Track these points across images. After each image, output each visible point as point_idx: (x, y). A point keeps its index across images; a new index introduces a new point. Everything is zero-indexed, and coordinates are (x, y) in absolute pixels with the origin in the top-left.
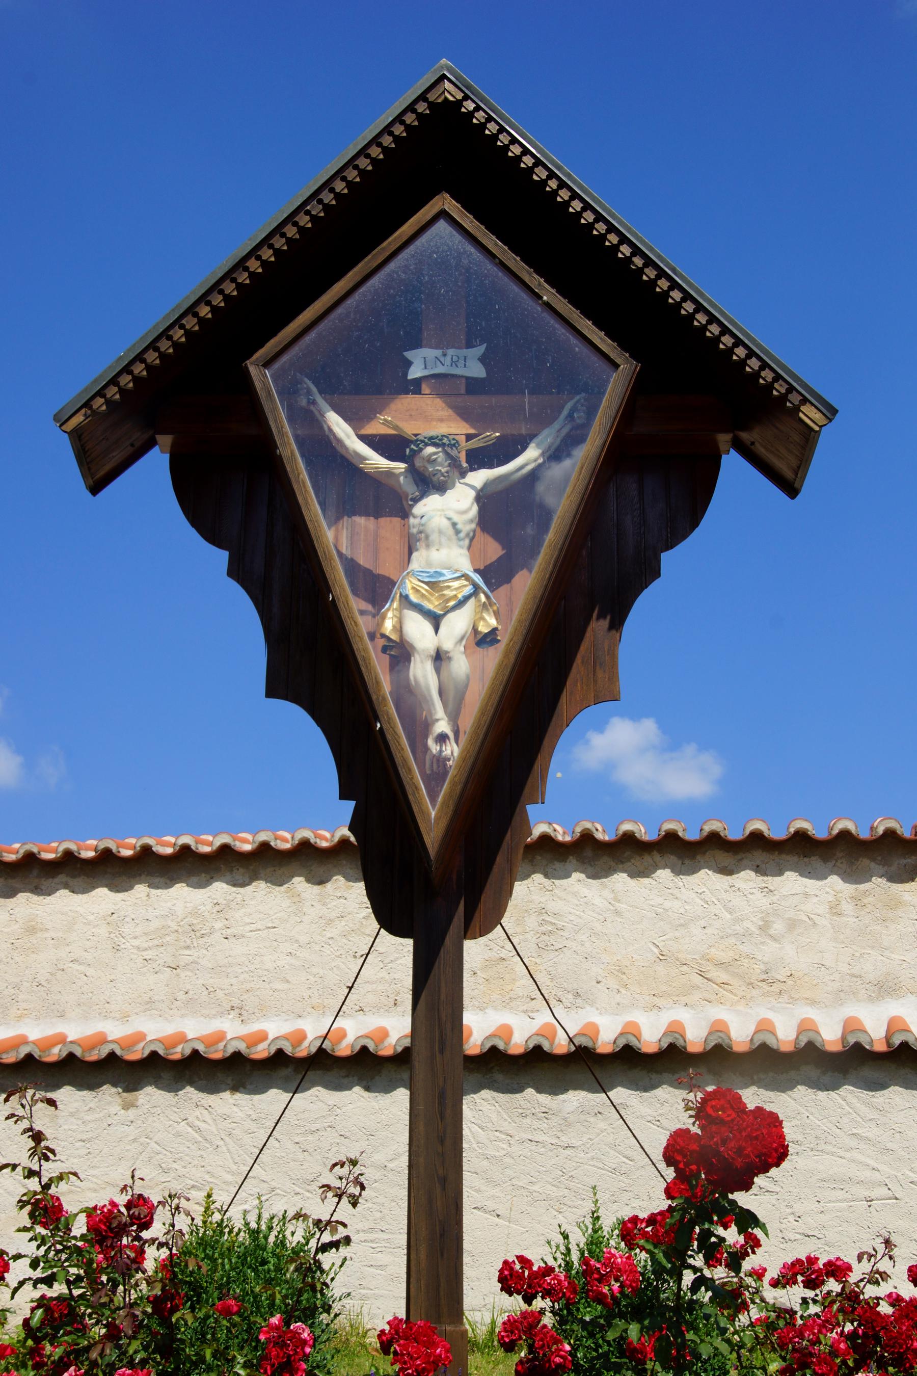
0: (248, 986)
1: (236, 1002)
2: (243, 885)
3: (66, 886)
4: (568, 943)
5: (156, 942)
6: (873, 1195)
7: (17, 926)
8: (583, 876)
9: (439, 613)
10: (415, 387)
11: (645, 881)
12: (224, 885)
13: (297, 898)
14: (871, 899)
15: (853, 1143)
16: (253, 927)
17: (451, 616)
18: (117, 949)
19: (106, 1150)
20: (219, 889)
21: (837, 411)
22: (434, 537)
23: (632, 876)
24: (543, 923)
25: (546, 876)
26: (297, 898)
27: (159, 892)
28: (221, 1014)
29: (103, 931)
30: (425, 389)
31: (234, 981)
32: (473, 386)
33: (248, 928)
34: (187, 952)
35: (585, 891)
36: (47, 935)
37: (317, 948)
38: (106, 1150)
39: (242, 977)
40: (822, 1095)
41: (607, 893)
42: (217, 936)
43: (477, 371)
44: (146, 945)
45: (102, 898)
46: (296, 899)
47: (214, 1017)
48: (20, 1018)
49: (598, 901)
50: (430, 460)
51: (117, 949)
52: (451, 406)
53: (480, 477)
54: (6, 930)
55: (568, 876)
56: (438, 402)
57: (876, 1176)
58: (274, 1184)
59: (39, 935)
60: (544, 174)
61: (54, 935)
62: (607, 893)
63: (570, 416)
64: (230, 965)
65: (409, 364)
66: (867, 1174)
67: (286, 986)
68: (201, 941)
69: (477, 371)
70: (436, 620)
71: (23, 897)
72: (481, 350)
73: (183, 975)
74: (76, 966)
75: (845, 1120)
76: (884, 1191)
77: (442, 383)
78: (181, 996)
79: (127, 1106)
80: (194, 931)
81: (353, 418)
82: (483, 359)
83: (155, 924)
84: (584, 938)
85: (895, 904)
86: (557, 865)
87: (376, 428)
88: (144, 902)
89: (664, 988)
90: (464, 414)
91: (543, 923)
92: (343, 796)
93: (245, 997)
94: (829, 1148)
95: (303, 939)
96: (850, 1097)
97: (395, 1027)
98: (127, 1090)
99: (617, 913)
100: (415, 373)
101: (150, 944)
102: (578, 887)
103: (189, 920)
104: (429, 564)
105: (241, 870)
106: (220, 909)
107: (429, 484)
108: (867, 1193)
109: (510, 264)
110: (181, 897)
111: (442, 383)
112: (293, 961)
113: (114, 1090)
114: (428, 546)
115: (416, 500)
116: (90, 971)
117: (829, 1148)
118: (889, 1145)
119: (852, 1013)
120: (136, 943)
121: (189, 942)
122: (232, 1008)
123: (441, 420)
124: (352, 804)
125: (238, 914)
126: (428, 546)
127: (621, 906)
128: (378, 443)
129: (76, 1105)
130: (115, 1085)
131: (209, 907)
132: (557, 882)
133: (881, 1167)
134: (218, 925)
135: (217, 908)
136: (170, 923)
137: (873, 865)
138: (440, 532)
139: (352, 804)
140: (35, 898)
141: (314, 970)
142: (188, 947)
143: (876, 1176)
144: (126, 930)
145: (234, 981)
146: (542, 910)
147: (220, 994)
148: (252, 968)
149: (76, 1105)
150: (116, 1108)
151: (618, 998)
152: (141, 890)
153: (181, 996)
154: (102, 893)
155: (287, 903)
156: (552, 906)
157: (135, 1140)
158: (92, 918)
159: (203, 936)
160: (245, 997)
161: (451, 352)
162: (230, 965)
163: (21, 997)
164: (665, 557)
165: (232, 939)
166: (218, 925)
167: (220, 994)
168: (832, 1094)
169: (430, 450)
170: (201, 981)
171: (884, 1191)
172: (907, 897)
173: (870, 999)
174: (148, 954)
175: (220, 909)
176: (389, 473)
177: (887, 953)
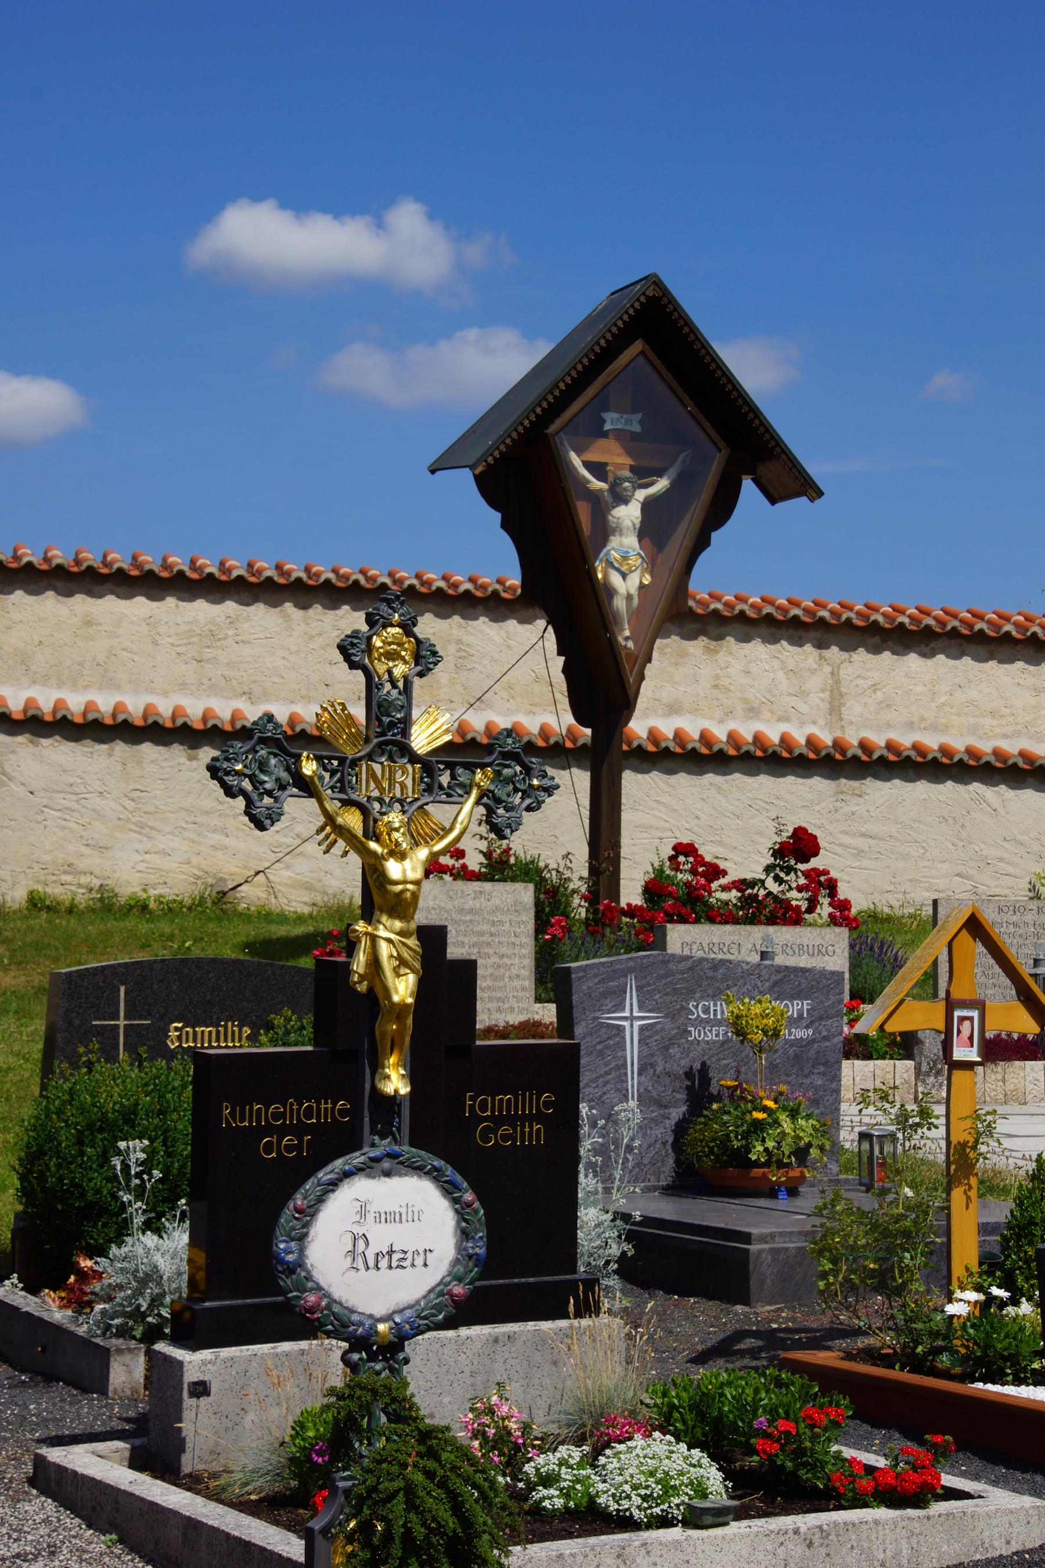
0: (255, 678)
1: (246, 689)
2: (248, 605)
3: (113, 593)
4: (477, 666)
5: (185, 641)
6: (664, 836)
7: (76, 619)
8: (487, 620)
9: (625, 570)
10: (605, 435)
11: (529, 626)
12: (234, 604)
13: (287, 617)
14: (669, 650)
15: (655, 805)
16: (256, 636)
17: (632, 575)
18: (155, 643)
19: (178, 787)
20: (230, 607)
21: (822, 494)
22: (625, 531)
23: (521, 622)
24: (460, 650)
25: (463, 617)
26: (287, 617)
27: (185, 604)
28: (237, 697)
29: (144, 629)
30: (611, 436)
31: (244, 674)
32: (634, 436)
33: (252, 637)
34: (208, 650)
35: (488, 630)
36: (100, 628)
37: (303, 655)
38: (178, 787)
39: (250, 672)
40: (640, 776)
41: (502, 633)
42: (230, 641)
43: (636, 428)
44: (177, 643)
45: (140, 606)
46: (287, 619)
47: (231, 698)
48: (86, 687)
49: (496, 638)
50: (625, 489)
51: (155, 643)
52: (623, 447)
53: (641, 494)
54: (69, 621)
55: (477, 619)
56: (617, 444)
57: (667, 825)
58: (295, 815)
59: (95, 627)
60: (682, 323)
61: (107, 629)
62: (502, 633)
63: (684, 461)
64: (241, 662)
65: (604, 421)
66: (662, 824)
67: (281, 680)
68: (218, 643)
69: (636, 428)
70: (624, 576)
71: (79, 598)
72: (639, 416)
73: (206, 666)
74: (125, 653)
75: (652, 792)
76: (670, 834)
77: (620, 435)
78: (205, 681)
79: (191, 759)
80: (213, 636)
81: (579, 456)
82: (641, 422)
83: (183, 628)
84: (486, 662)
85: (683, 654)
86: (470, 610)
87: (591, 457)
88: (171, 610)
89: (537, 700)
90: (629, 453)
91: (460, 650)
92: (559, 654)
93: (252, 686)
94: (641, 808)
95: (293, 648)
96: (656, 779)
97: (636, 787)
98: (191, 748)
99: (509, 647)
100: (607, 427)
101: (181, 642)
102: (483, 627)
103: (210, 626)
104: (622, 545)
105: (246, 594)
106: (232, 622)
107: (623, 499)
108: (660, 835)
109: (651, 358)
110: (201, 609)
111: (620, 435)
112: (286, 663)
113: (181, 747)
114: (621, 535)
115: (614, 507)
116: (136, 658)
117: (641, 808)
118: (676, 807)
119: (654, 724)
120: (170, 640)
121: (209, 643)
122: (244, 693)
123: (618, 455)
124: (563, 658)
125: (245, 626)
126: (621, 535)
127: (512, 643)
128: (587, 465)
129: (155, 755)
130: (182, 744)
131: (223, 618)
132: (470, 622)
133: (671, 820)
134: (230, 633)
135: (229, 620)
136: (195, 628)
137: (673, 627)
138: (628, 528)
139: (563, 658)
140: (89, 599)
141: (302, 671)
142: (208, 647)
143: (667, 825)
144: (162, 629)
145: (244, 674)
146: (459, 642)
147: (234, 682)
148: (257, 665)
149: (155, 755)
150: (183, 759)
151: (508, 705)
152: (171, 601)
153: (205, 681)
154: (141, 600)
155: (280, 621)
156: (466, 639)
157: (199, 781)
158: (135, 619)
159: (219, 639)
160: (252, 686)
161: (625, 416)
162: (241, 662)
163: (85, 672)
164: (713, 534)
165: (241, 644)
166: (230, 633)
167: (234, 682)
168: (646, 776)
169: (627, 484)
170: (219, 672)
171: (670, 834)
172: (691, 650)
173: (665, 715)
174: (180, 650)
175: (232, 622)
176: (601, 490)
177: (676, 686)
